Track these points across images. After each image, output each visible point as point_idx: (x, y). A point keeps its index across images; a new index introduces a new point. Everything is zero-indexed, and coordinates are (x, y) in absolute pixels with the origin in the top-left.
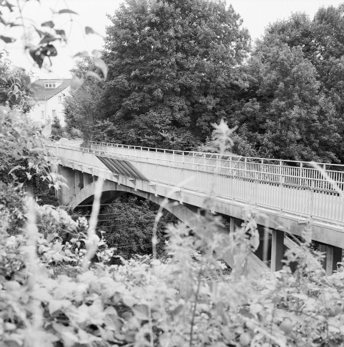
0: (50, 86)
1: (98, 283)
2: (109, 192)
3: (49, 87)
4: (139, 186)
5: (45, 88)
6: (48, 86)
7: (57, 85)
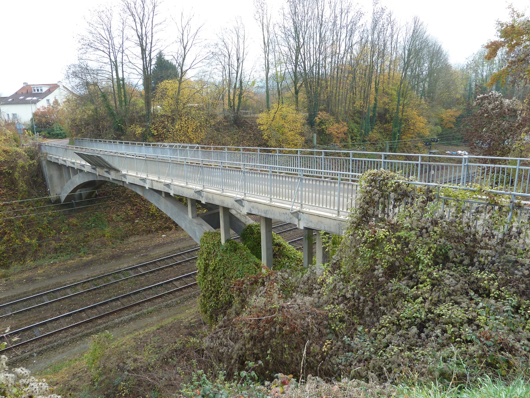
0: (38, 90)
1: (249, 214)
2: (95, 181)
3: (36, 92)
4: (112, 176)
5: (33, 92)
6: (40, 90)
7: (45, 89)
